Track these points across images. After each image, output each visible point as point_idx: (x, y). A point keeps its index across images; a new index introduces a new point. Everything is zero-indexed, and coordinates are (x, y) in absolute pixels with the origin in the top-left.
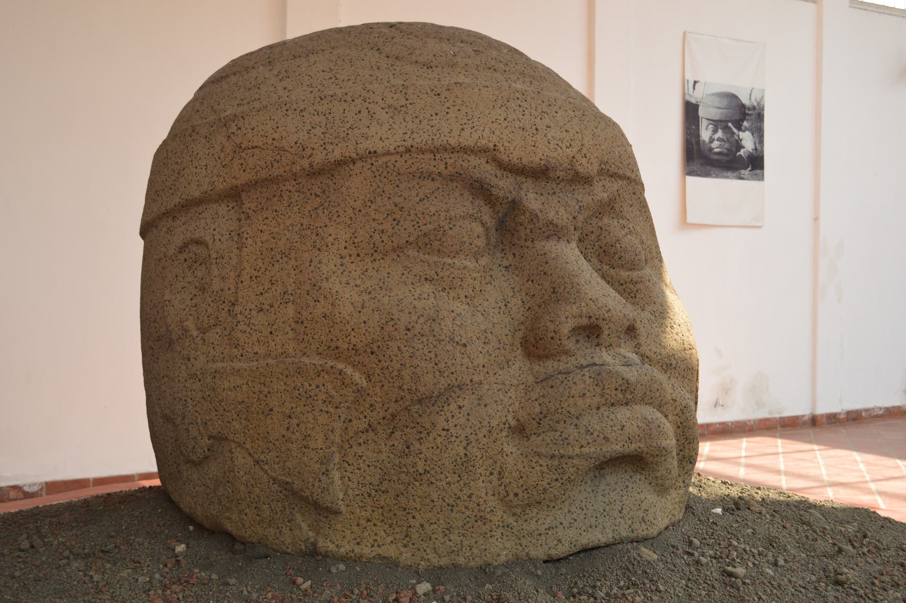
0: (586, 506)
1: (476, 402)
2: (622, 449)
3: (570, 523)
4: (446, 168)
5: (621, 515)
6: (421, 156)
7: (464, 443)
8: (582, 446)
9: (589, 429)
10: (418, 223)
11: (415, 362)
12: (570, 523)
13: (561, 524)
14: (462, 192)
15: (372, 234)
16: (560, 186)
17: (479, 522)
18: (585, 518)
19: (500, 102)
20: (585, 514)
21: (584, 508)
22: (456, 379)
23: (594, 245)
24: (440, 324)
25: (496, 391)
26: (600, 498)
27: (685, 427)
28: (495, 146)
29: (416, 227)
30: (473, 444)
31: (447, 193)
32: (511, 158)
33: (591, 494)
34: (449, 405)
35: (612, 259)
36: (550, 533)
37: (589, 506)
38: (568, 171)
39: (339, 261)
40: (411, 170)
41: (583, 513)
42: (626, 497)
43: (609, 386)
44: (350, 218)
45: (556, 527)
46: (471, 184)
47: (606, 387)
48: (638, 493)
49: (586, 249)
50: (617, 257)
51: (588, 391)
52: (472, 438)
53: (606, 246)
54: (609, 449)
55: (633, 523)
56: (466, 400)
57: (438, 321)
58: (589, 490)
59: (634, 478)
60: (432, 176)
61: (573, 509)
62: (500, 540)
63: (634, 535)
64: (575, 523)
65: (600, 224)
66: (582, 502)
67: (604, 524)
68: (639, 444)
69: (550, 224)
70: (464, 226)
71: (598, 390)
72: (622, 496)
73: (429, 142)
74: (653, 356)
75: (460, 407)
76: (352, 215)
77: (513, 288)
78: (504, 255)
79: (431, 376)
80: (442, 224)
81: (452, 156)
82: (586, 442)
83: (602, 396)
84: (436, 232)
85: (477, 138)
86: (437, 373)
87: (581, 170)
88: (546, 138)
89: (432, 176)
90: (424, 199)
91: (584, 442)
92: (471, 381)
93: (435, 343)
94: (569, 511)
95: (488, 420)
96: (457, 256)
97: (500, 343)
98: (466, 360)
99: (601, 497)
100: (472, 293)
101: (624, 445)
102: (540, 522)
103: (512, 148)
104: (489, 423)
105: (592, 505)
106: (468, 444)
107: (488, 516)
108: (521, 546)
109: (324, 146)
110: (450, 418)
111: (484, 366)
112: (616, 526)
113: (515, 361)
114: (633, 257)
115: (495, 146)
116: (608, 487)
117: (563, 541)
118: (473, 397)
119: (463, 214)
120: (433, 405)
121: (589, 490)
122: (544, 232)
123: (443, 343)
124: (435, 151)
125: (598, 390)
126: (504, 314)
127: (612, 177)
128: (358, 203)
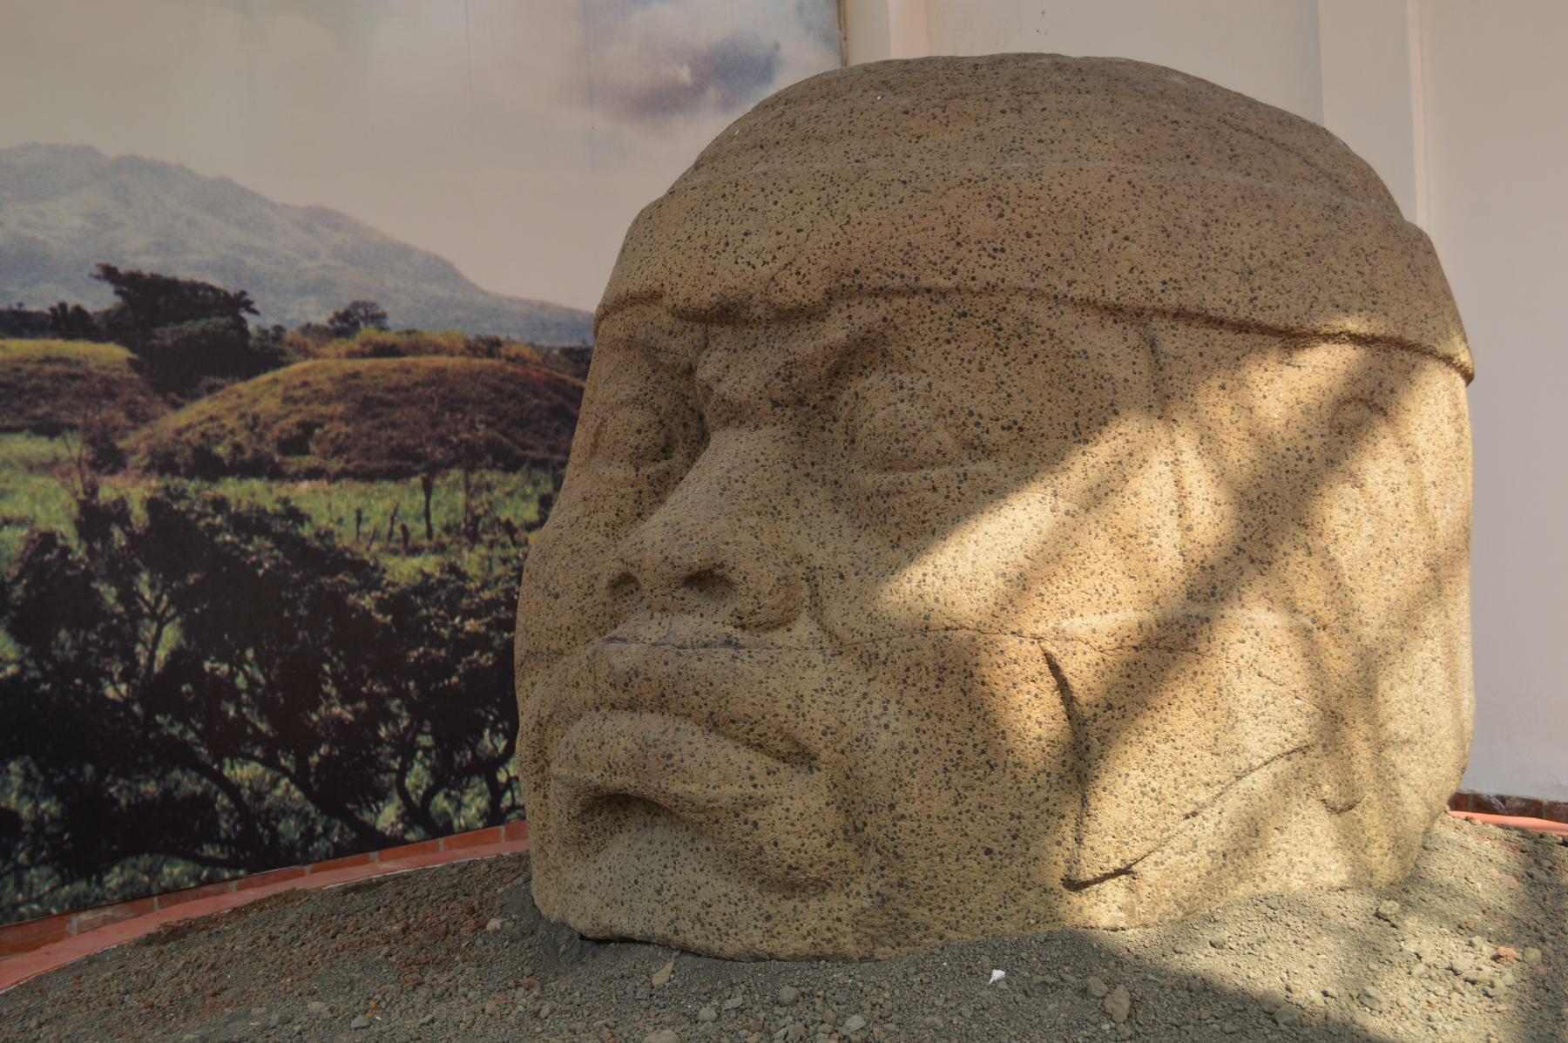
5: (659, 898)
42: (670, 870)
55: (678, 918)
63: (679, 939)
68: (627, 778)
72: (666, 867)
74: (847, 636)
92: (548, 649)
100: (615, 518)
111: (569, 628)
114: (885, 446)
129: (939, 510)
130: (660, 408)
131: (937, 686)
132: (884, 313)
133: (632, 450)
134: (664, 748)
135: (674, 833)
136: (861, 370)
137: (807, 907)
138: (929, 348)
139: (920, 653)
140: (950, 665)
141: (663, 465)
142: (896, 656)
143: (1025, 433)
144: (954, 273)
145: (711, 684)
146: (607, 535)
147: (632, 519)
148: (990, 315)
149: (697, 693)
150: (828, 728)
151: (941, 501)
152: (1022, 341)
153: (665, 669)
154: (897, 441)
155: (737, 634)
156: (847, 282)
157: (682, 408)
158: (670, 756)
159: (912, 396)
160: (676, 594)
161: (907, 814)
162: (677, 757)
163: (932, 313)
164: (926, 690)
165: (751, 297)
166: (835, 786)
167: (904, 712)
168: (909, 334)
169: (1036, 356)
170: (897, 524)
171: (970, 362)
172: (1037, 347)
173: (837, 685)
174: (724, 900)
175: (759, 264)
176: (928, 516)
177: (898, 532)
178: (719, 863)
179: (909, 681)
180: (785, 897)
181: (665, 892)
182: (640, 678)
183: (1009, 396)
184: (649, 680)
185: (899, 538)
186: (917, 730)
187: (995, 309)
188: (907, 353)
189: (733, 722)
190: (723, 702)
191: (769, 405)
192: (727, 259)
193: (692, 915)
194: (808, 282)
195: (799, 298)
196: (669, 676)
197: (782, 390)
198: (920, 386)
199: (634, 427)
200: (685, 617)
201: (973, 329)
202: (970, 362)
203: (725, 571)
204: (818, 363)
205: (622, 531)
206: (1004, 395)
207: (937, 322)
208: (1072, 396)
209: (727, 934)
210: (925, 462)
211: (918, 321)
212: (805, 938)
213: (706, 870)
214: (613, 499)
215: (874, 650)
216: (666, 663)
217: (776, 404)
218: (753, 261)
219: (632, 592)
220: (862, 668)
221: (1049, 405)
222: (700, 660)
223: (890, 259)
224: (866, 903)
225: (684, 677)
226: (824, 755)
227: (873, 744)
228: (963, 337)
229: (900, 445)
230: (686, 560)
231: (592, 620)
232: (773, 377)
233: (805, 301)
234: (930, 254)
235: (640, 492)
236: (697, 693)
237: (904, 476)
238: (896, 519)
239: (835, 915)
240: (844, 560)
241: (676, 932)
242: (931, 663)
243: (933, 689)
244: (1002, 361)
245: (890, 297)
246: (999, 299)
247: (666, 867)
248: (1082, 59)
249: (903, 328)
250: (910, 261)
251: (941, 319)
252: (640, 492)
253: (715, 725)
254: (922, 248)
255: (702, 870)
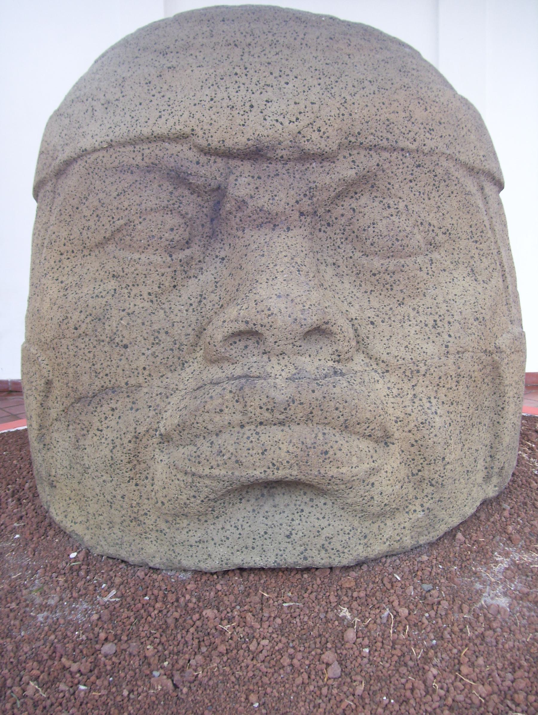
0: (242, 526)
1: (129, 405)
2: (263, 476)
3: (222, 541)
4: (143, 160)
6: (123, 149)
7: (111, 446)
8: (212, 467)
9: (222, 449)
10: (113, 218)
11: (78, 361)
12: (222, 541)
13: (213, 539)
14: (161, 183)
15: (82, 231)
16: (287, 167)
17: (134, 523)
18: (239, 538)
19: (211, 81)
20: (240, 534)
21: (240, 527)
22: (110, 381)
23: (344, 230)
24: (104, 324)
25: (154, 395)
26: (260, 519)
27: (422, 446)
28: (193, 130)
29: (111, 222)
30: (118, 448)
31: (145, 185)
32: (210, 142)
33: (251, 513)
34: (101, 406)
35: (364, 246)
36: (200, 546)
37: (246, 526)
38: (291, 149)
39: (58, 257)
40: (113, 165)
41: (238, 532)
42: (297, 522)
43: (252, 404)
44: (70, 215)
45: (207, 541)
46: (168, 174)
47: (248, 404)
48: (318, 519)
49: (335, 234)
50: (369, 242)
51: (227, 407)
52: (118, 442)
53: (358, 230)
54: (244, 474)
56: (119, 403)
57: (103, 321)
58: (250, 509)
59: (316, 502)
60: (131, 169)
61: (228, 526)
62: (154, 542)
64: (227, 541)
65: (353, 206)
66: (238, 520)
67: (264, 547)
69: (260, 210)
70: (154, 220)
71: (239, 407)
73: (125, 134)
74: (393, 361)
75: (113, 410)
76: (71, 213)
77: (217, 282)
78: (222, 246)
79: (87, 376)
80: (132, 218)
81: (150, 145)
82: (216, 463)
83: (244, 413)
84: (127, 227)
85: (172, 124)
86: (94, 374)
87: (308, 146)
88: (261, 114)
89: (131, 169)
90: (121, 193)
91: (214, 463)
92: (127, 384)
93: (95, 343)
94: (223, 528)
95: (134, 425)
96: (146, 250)
97: (175, 344)
98: (124, 362)
99: (261, 518)
100: (157, 289)
101: (265, 471)
102: (191, 533)
103: (213, 131)
104: (135, 428)
105: (250, 526)
106: (114, 448)
107: (141, 518)
108: (174, 552)
109: (321, 133)
110: (103, 419)
111: (144, 369)
112: (280, 550)
113: (193, 362)
115: (193, 130)
116: (274, 509)
117: (213, 557)
118: (127, 400)
119: (155, 206)
120: (89, 405)
121: (250, 509)
122: (255, 220)
123: (102, 344)
124: (133, 142)
125: (239, 407)
126: (194, 311)
127: (370, 150)
128: (75, 200)
129: (425, 282)
130: (187, 214)
131: (456, 386)
132: (378, 161)
133: (168, 243)
134: (321, 448)
135: (294, 498)
136: (353, 194)
137: (386, 524)
138: (402, 184)
139: (447, 368)
140: (463, 373)
141: (188, 252)
142: (432, 370)
143: (451, 236)
144: (415, 141)
145: (346, 402)
146: (152, 301)
147: (170, 289)
148: (432, 168)
149: (337, 409)
150: (397, 418)
151: (425, 276)
152: (446, 183)
153: (314, 395)
154: (397, 240)
155: (338, 366)
156: (353, 139)
157: (201, 214)
158: (326, 453)
159: (398, 212)
160: (296, 344)
161: (450, 461)
162: (331, 452)
163: (403, 163)
164: (451, 389)
165: (279, 144)
166: (403, 451)
167: (440, 403)
168: (390, 175)
169: (452, 192)
170: (402, 291)
171: (423, 194)
172: (453, 188)
173: (395, 391)
174: (341, 533)
175: (286, 122)
176: (420, 285)
177: (402, 295)
178: (335, 511)
179: (441, 385)
180: (373, 523)
181: (294, 535)
182: (296, 404)
183: (443, 215)
184: (301, 404)
185: (404, 299)
186: (448, 412)
187: (434, 164)
188: (389, 186)
189: (358, 424)
190: (354, 413)
191: (298, 214)
192: (254, 117)
193: (318, 546)
194: (328, 137)
195: (323, 146)
196: (317, 400)
197: (309, 205)
198: (401, 206)
199: (168, 227)
200: (299, 357)
201: (423, 175)
202: (423, 194)
203: (329, 326)
204: (332, 189)
205: (163, 299)
206: (441, 214)
207: (406, 169)
208: (469, 216)
209: (344, 553)
210: (412, 253)
211: (396, 168)
212: (385, 543)
213: (327, 517)
214: (155, 277)
215: (416, 368)
216: (313, 391)
217: (302, 214)
218: (281, 119)
219: (235, 343)
220: (406, 380)
221: (460, 221)
222: (334, 387)
223: (378, 128)
224: (421, 515)
225: (328, 398)
226: (397, 435)
227: (434, 424)
228: (418, 179)
229: (400, 242)
230: (309, 321)
231: (164, 361)
232: (302, 196)
233: (327, 149)
234: (400, 127)
235: (175, 271)
236: (337, 409)
237: (402, 261)
238: (401, 287)
239: (402, 526)
240: (370, 313)
241: (305, 558)
242: (454, 373)
243: (454, 388)
244: (437, 195)
245: (379, 151)
246: (435, 158)
247: (293, 520)
248: (136, 32)
249: (387, 171)
250: (391, 131)
251: (408, 167)
252: (175, 271)
253: (346, 427)
254: (396, 123)
255: (324, 518)
